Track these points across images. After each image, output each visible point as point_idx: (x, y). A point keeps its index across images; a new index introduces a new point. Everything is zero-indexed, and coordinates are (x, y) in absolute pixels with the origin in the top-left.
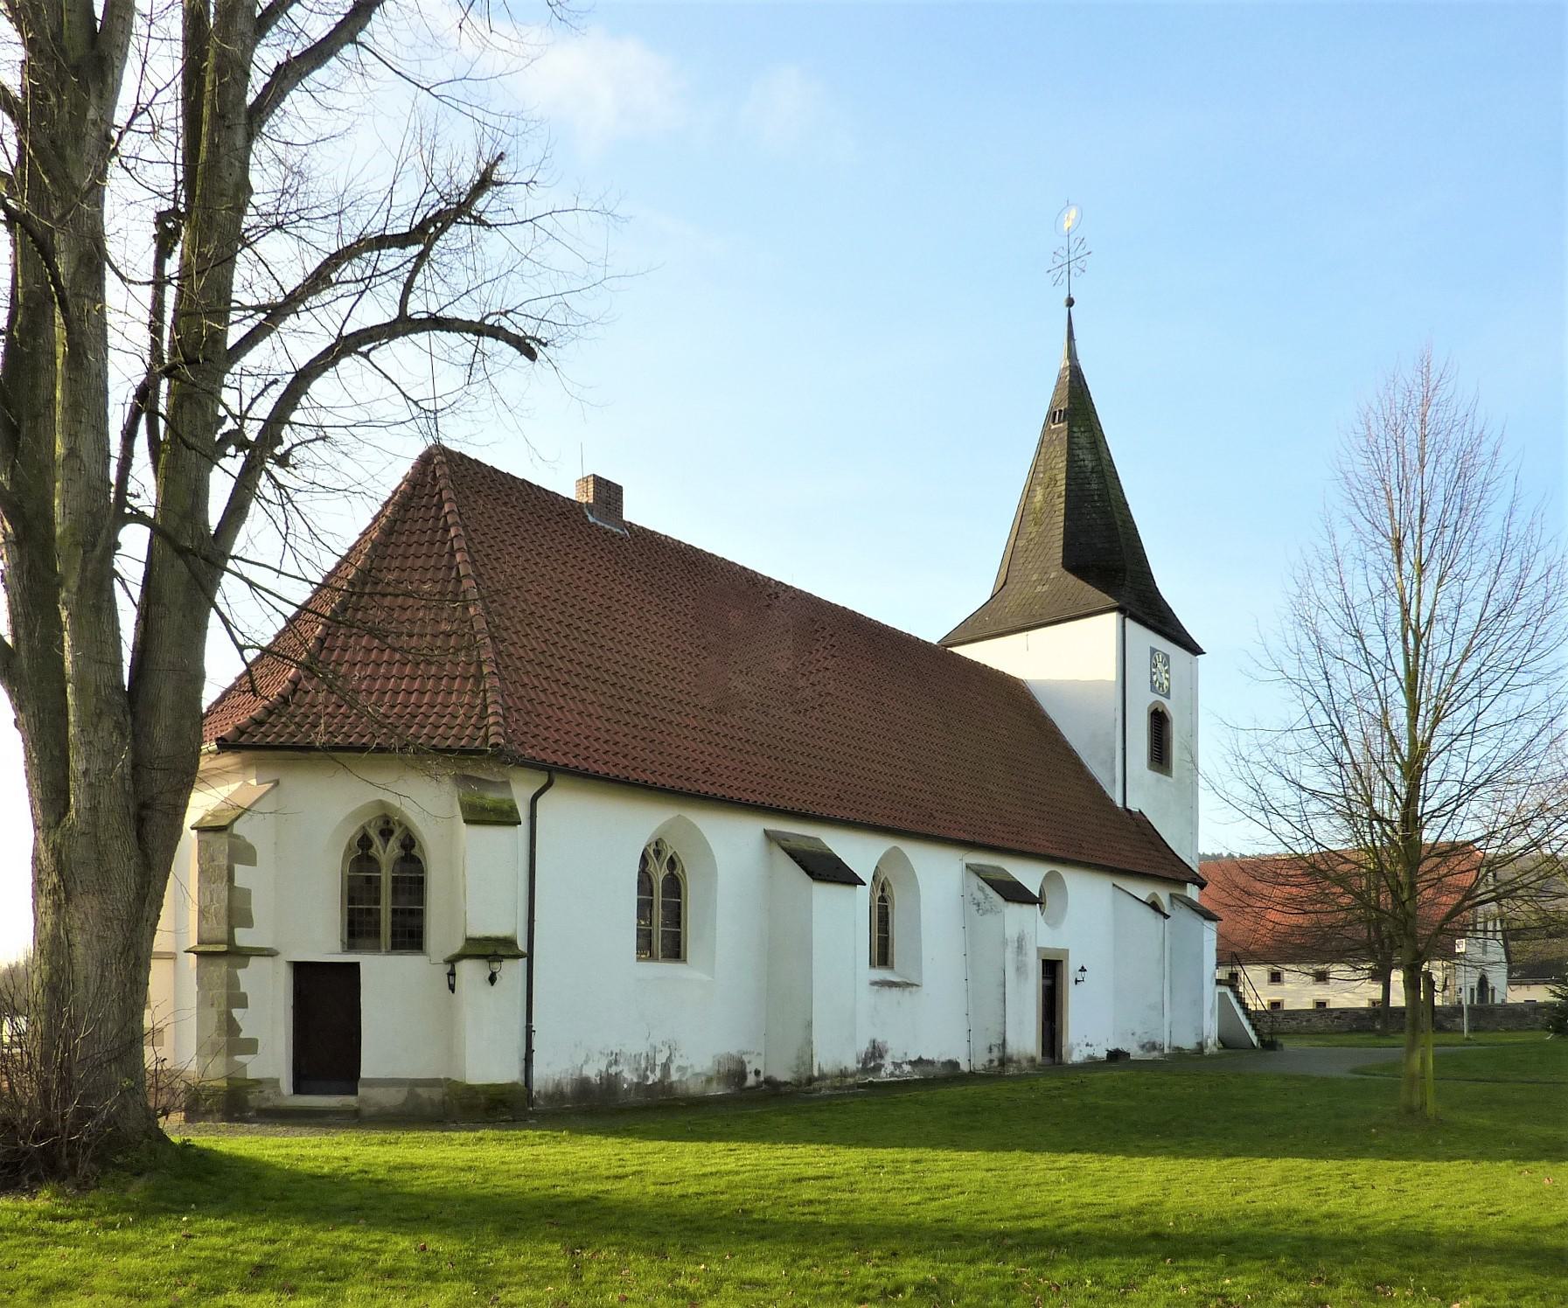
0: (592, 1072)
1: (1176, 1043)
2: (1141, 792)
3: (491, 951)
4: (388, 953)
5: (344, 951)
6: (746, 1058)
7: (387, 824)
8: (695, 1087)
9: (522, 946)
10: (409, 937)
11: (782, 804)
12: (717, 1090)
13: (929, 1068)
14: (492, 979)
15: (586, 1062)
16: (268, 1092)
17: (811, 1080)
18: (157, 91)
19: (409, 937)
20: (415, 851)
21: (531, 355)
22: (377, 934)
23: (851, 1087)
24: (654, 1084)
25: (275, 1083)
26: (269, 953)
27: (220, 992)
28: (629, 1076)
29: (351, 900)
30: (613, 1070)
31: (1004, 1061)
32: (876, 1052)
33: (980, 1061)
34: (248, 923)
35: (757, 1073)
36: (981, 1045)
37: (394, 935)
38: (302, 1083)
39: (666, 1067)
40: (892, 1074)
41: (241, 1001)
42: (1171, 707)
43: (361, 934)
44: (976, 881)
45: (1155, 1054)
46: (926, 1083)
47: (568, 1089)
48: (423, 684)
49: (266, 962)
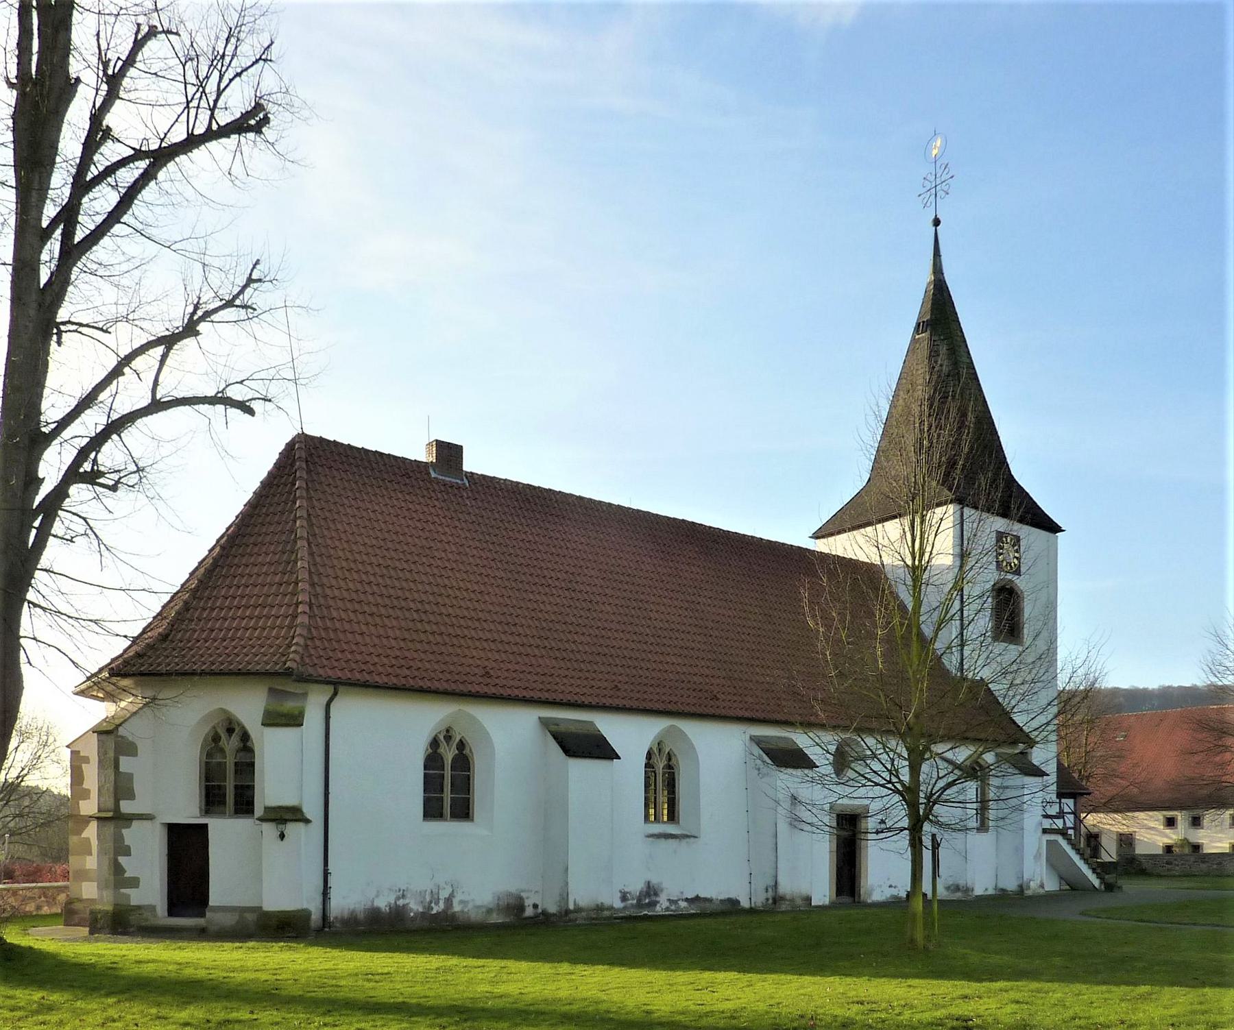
0: (383, 903)
1: (1001, 886)
2: (985, 662)
3: (285, 816)
4: (231, 817)
5: (202, 816)
6: (524, 895)
7: (232, 726)
8: (475, 916)
9: (312, 810)
10: (244, 805)
11: (559, 697)
12: (496, 919)
13: (707, 905)
14: (282, 836)
15: (377, 896)
16: (147, 914)
17: (567, 912)
18: (272, 144)
19: (244, 805)
20: (249, 744)
21: (251, 412)
22: (223, 803)
23: (605, 919)
24: (438, 913)
25: (152, 908)
26: (148, 817)
27: (110, 845)
28: (415, 907)
29: (207, 779)
30: (401, 902)
31: (777, 899)
32: (651, 891)
33: (759, 899)
34: (131, 795)
35: (535, 906)
36: (761, 883)
37: (236, 803)
38: (172, 911)
39: (449, 901)
40: (667, 909)
41: (127, 852)
42: (1021, 583)
43: (213, 804)
44: (757, 751)
45: (958, 895)
46: (702, 915)
47: (361, 916)
48: (257, 622)
49: (146, 824)
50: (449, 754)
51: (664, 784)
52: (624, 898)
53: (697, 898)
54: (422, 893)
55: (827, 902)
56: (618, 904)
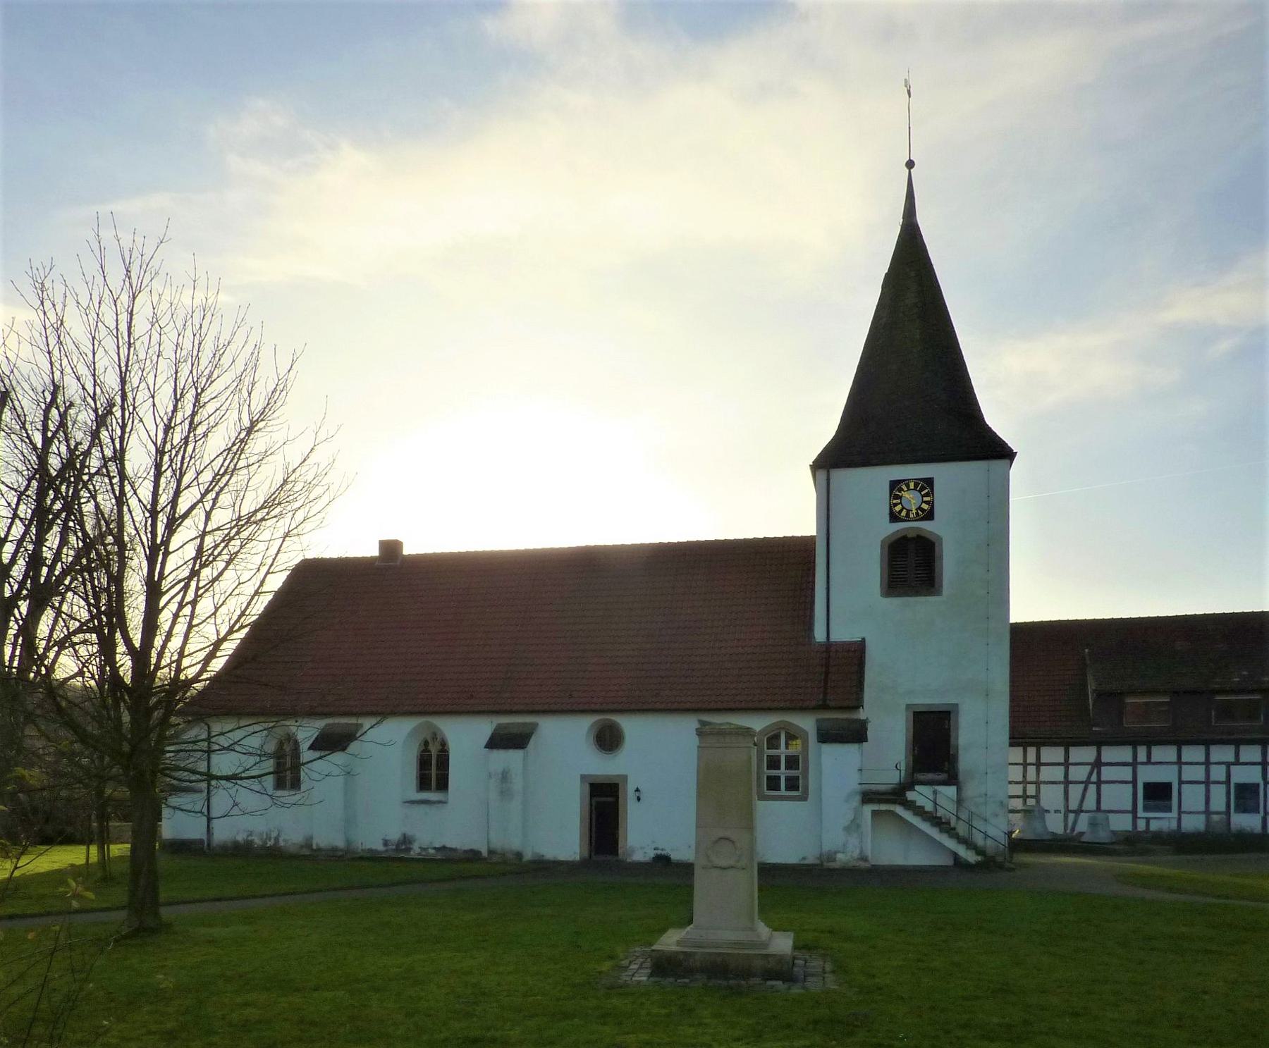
28: (257, 841)
32: (406, 841)
39: (277, 839)
50: (434, 750)
51: (433, 771)
52: (386, 843)
53: (444, 848)
54: (261, 834)
55: (578, 858)
56: (380, 847)
